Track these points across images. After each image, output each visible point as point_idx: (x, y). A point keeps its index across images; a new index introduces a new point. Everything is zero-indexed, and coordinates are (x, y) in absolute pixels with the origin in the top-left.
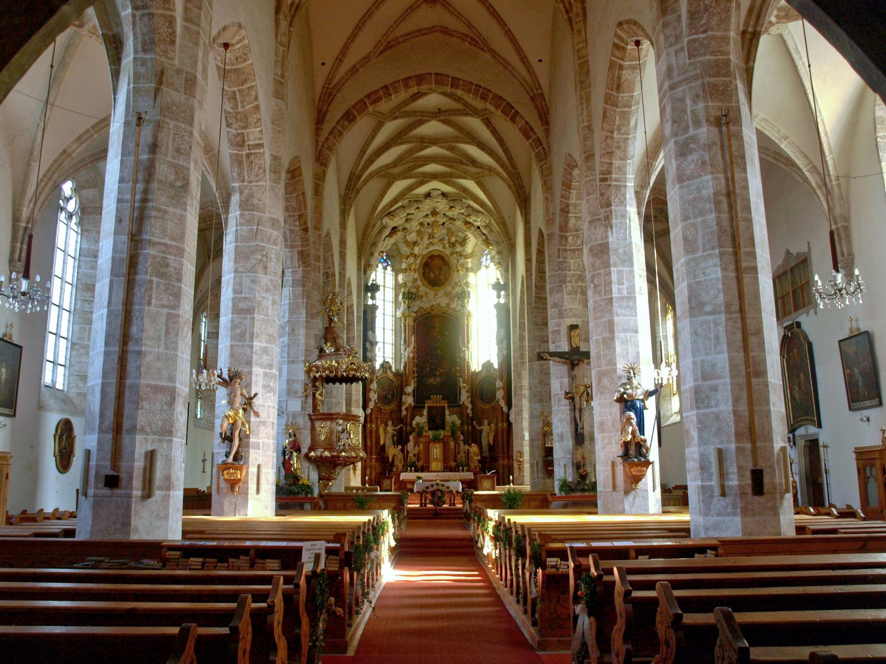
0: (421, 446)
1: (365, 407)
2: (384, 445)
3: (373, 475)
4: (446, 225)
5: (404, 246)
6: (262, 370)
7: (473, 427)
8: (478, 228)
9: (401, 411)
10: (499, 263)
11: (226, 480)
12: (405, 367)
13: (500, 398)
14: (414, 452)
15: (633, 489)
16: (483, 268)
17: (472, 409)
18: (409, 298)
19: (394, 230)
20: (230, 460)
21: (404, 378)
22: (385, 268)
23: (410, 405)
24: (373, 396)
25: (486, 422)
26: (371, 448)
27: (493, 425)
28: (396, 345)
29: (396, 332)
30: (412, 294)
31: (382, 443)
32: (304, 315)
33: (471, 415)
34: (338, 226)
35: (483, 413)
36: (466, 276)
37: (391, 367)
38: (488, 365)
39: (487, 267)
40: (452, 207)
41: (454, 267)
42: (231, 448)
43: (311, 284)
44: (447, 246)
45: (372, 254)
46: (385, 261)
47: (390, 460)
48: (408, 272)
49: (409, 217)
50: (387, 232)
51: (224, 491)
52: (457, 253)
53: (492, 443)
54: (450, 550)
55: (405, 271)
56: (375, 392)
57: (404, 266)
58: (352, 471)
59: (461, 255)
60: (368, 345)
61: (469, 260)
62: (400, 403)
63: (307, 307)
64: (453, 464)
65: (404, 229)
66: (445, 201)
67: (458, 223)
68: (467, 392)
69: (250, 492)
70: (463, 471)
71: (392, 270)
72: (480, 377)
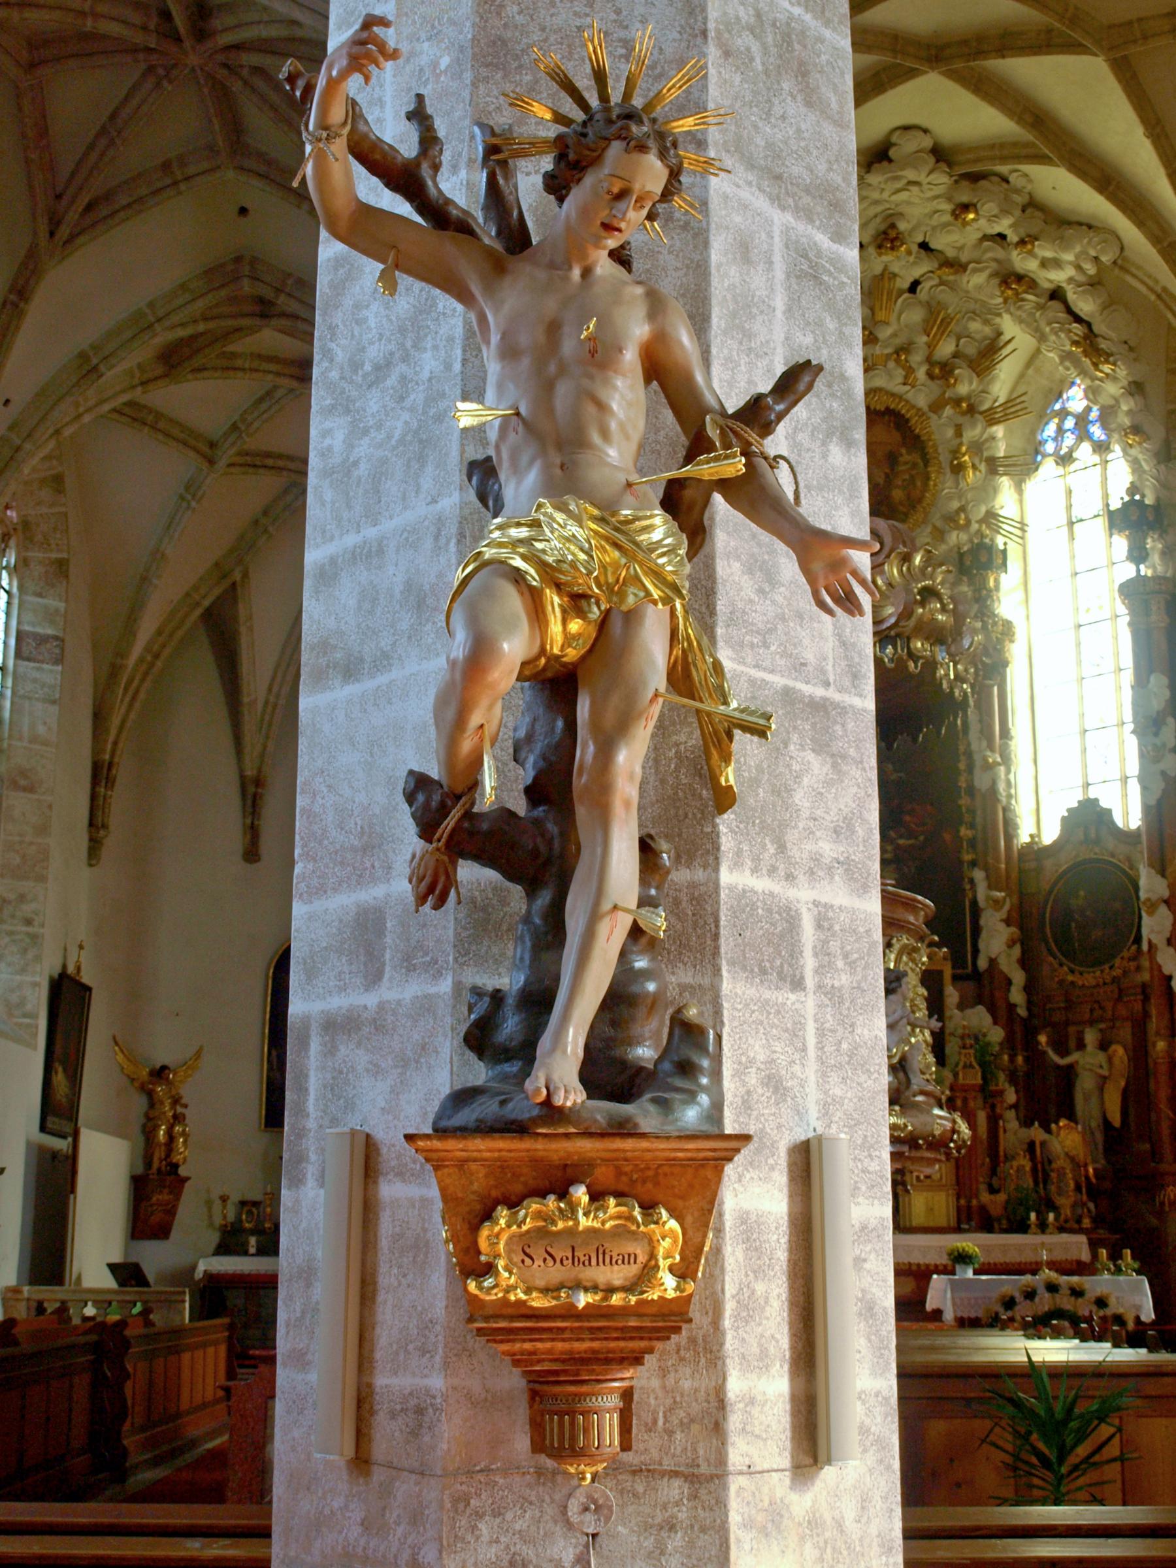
4: (923, 291)
6: (781, 219)
7: (1035, 1056)
8: (1056, 295)
10: (1136, 429)
11: (500, 1325)
13: (1159, 940)
16: (1048, 467)
17: (1028, 988)
20: (561, 1070)
25: (1091, 1037)
27: (1119, 1051)
33: (1022, 1012)
35: (1070, 1005)
36: (988, 490)
38: (1088, 818)
39: (1065, 459)
40: (965, 207)
41: (944, 458)
42: (550, 933)
44: (921, 374)
51: (448, 1435)
52: (957, 402)
53: (1116, 1119)
54: (567, 1436)
59: (972, 410)
61: (999, 431)
64: (995, 1203)
66: (942, 180)
67: (975, 280)
68: (1008, 922)
69: (738, 1453)
70: (1043, 1227)
72: (1065, 861)
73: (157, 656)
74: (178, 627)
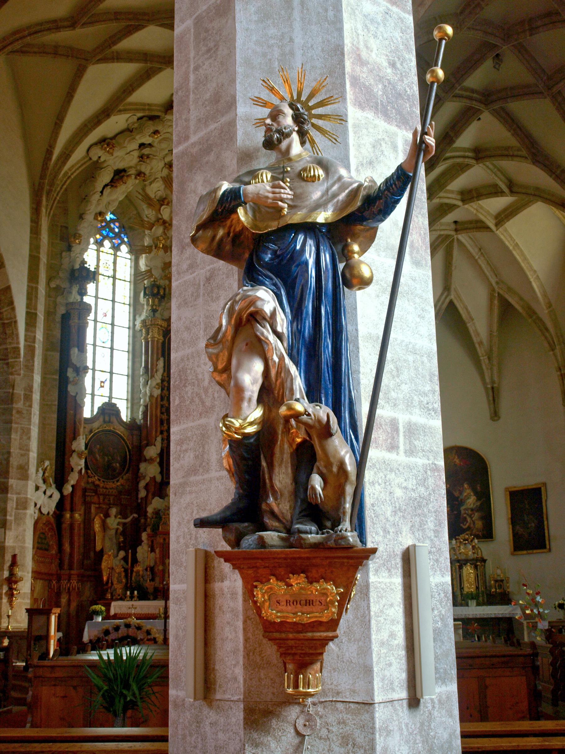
0: (157, 551)
1: (60, 478)
2: (102, 551)
3: (74, 605)
5: (145, 206)
9: (137, 491)
12: (145, 413)
14: (147, 563)
15: (296, 700)
18: (154, 295)
19: (120, 175)
21: (144, 433)
22: (116, 248)
23: (154, 479)
24: (78, 463)
26: (71, 555)
28: (133, 377)
29: (134, 353)
30: (158, 287)
31: (98, 547)
37: (117, 412)
45: (81, 217)
46: (117, 236)
48: (154, 251)
49: (146, 151)
50: (106, 177)
55: (148, 250)
56: (80, 455)
57: (147, 241)
60: (70, 373)
62: (137, 477)
65: (139, 174)
71: (130, 252)
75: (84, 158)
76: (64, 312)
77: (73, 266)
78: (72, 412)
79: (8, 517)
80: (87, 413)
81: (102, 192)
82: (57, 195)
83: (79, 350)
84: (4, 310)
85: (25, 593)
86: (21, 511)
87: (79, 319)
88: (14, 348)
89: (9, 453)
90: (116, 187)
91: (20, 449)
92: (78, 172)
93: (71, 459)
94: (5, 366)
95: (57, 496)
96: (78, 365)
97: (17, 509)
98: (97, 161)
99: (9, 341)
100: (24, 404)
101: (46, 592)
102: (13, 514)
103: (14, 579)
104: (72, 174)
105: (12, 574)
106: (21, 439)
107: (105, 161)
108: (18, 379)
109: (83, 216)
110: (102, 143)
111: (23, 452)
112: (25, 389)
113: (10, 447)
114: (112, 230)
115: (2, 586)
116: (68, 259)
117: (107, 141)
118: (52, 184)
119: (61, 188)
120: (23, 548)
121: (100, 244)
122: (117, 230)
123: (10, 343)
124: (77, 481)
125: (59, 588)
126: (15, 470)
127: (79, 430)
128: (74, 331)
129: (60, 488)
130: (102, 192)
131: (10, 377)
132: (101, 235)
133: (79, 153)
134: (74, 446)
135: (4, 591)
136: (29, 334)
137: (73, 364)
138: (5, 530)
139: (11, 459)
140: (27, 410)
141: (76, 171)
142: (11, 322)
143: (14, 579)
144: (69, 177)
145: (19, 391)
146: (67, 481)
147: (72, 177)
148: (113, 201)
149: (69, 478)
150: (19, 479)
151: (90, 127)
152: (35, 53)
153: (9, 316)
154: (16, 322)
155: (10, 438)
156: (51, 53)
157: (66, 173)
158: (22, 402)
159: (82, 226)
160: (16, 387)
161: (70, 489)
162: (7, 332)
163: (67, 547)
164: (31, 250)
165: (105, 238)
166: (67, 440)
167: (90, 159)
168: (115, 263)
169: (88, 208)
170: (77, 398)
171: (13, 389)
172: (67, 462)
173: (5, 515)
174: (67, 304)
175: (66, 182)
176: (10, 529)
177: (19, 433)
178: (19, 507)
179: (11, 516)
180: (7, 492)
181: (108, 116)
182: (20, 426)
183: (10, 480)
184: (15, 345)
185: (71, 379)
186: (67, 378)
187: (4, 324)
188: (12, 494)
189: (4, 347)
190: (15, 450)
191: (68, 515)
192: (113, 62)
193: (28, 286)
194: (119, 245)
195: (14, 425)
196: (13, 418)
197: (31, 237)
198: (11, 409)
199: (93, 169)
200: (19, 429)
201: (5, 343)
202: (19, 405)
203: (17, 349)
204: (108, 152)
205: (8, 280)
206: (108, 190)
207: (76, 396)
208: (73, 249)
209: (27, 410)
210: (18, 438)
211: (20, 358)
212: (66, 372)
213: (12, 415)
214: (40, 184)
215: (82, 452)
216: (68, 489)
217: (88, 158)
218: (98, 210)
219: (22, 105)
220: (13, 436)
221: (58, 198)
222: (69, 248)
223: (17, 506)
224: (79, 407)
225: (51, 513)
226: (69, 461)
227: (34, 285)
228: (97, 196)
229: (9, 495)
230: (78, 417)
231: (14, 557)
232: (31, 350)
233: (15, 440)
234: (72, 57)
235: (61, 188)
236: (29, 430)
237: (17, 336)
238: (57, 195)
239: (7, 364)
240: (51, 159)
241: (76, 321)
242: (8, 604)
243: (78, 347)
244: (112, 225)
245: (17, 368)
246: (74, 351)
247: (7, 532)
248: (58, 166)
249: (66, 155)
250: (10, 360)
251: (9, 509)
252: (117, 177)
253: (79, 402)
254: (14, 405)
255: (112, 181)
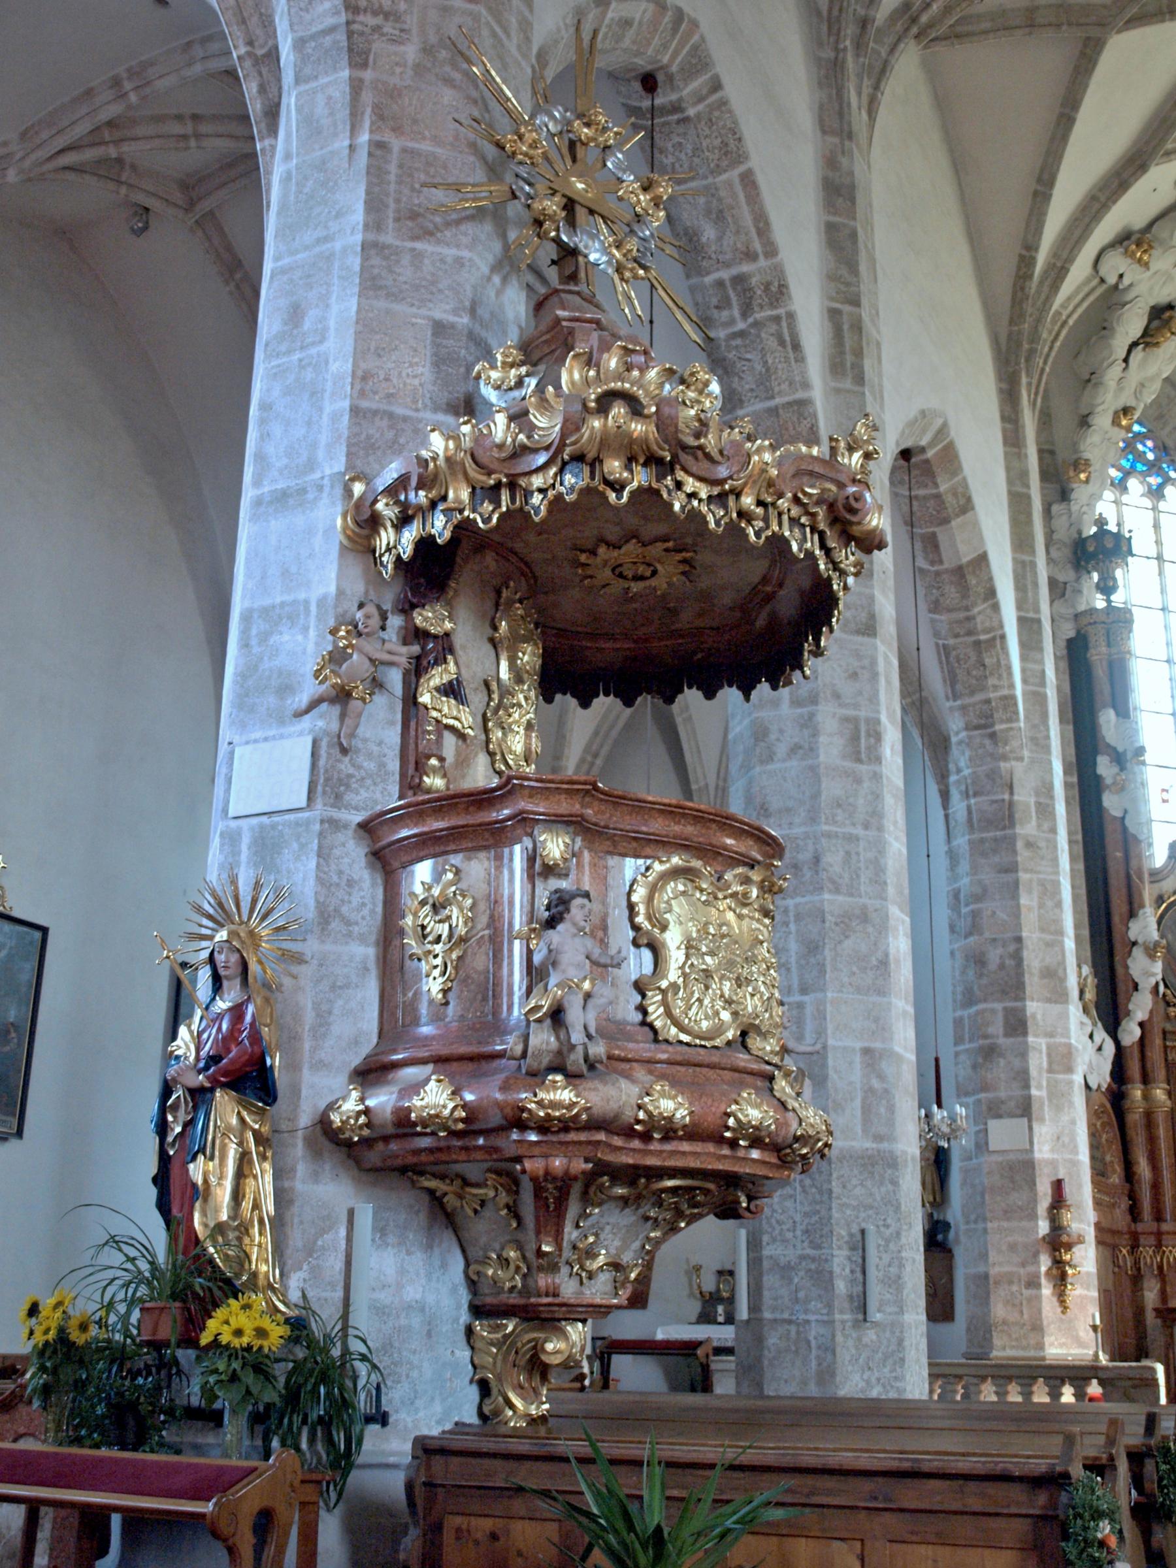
1: (1109, 1008)
24: (1147, 971)
26: (1156, 1186)
32: (358, 215)
34: (805, 119)
43: (411, 52)
45: (1084, 422)
46: (1154, 467)
47: (200, 1182)
50: (1132, 324)
56: (1151, 952)
58: (1047, 1290)
60: (1104, 767)
63: (376, 173)
73: (596, 756)
74: (612, 727)
75: (1088, 280)
76: (1072, 634)
77: (1080, 532)
78: (1119, 854)
79: (1034, 1092)
80: (1159, 856)
81: (1126, 360)
82: (1045, 363)
83: (1118, 714)
84: (976, 610)
85: (1088, 1274)
86: (1061, 1076)
87: (1109, 645)
88: (1005, 698)
89: (1019, 940)
90: (1157, 344)
91: (1042, 930)
92: (1080, 311)
93: (1129, 962)
94: (987, 742)
95: (1110, 1048)
96: (1120, 749)
97: (1050, 1070)
98: (1116, 287)
99: (991, 681)
100: (1039, 826)
101: (1111, 1276)
102: (1044, 1083)
103: (1065, 1238)
104: (1069, 316)
105: (1057, 1228)
106: (1041, 906)
107: (1131, 285)
108: (1018, 768)
109: (1090, 419)
110: (1125, 243)
111: (1048, 937)
112: (1037, 794)
113: (1018, 926)
114: (1140, 457)
115: (1036, 1255)
116: (1064, 518)
117: (1134, 238)
118: (1035, 337)
119: (1051, 348)
120: (1075, 1163)
121: (1121, 486)
122: (1150, 456)
123: (996, 687)
124: (1151, 1012)
125: (1136, 1263)
126: (1036, 979)
127: (1141, 896)
128: (1100, 672)
129: (1113, 1026)
130: (1126, 360)
131: (1002, 764)
132: (1120, 468)
133: (1080, 270)
134: (1135, 930)
135: (1043, 1269)
136: (1030, 666)
137: (1108, 745)
138: (1030, 1121)
139: (1025, 954)
140: (1048, 840)
141: (1076, 308)
142: (994, 639)
143: (1065, 1238)
144: (1065, 322)
145: (1024, 796)
146: (1128, 1013)
147: (1071, 322)
148: (1152, 379)
149: (1131, 1007)
150: (1049, 1001)
151: (1103, 199)
152: (986, 32)
153: (987, 624)
154: (1003, 637)
155: (1018, 906)
156: (1020, 27)
157: (1058, 313)
158: (1034, 822)
159: (1089, 441)
160: (1016, 790)
161: (1138, 1032)
162: (987, 661)
163: (1143, 1168)
164: (1010, 482)
165: (1127, 474)
166: (1116, 919)
167: (1102, 281)
168: (1156, 526)
169: (1099, 401)
170: (1127, 822)
171: (1012, 793)
172: (1120, 971)
173: (1027, 1086)
174: (1076, 616)
175: (1058, 335)
176: (1042, 1120)
177: (1035, 894)
178: (1055, 1067)
179: (1039, 1087)
180: (1025, 1033)
181: (1143, 168)
182: (1035, 876)
183: (1028, 1003)
184: (1005, 692)
185: (1109, 781)
186: (1098, 779)
187: (978, 643)
188: (1036, 1036)
189: (979, 697)
190: (1031, 934)
191: (1138, 1094)
192: (1163, 21)
193: (1015, 560)
194: (1161, 487)
195: (1023, 876)
196: (1019, 859)
197: (1006, 454)
198: (1012, 840)
199: (1111, 299)
200: (1035, 884)
201: (983, 688)
202: (1027, 828)
203: (1009, 701)
204: (1140, 260)
205: (981, 539)
206: (1138, 355)
207: (1123, 818)
208: (1073, 496)
209: (1048, 840)
210: (1035, 904)
211: (1018, 720)
212: (1095, 764)
213: (1015, 852)
214: (1010, 335)
215: (1156, 945)
216: (1131, 1032)
217: (1096, 281)
218: (1120, 404)
219: (960, 165)
220: (1024, 901)
221: (1047, 369)
222: (1064, 495)
223: (1050, 1063)
224: (1131, 843)
225: (1104, 1086)
226: (1127, 967)
227: (1027, 558)
228: (1117, 370)
229: (1031, 1039)
230: (1134, 864)
231: (1058, 1185)
232: (1037, 699)
233: (1030, 909)
234: (1070, 24)
235: (1051, 348)
236: (1057, 884)
237: (1009, 668)
238: (1045, 363)
239: (993, 736)
240: (1031, 276)
241: (1104, 649)
242: (1055, 1299)
243: (1114, 707)
244: (1140, 447)
245: (1015, 743)
246: (1107, 719)
247: (1035, 1126)
248: (1043, 296)
249: (1058, 272)
250: (998, 727)
251: (1033, 1072)
252: (1156, 323)
253: (1132, 829)
254: (1019, 830)
255: (1146, 333)
